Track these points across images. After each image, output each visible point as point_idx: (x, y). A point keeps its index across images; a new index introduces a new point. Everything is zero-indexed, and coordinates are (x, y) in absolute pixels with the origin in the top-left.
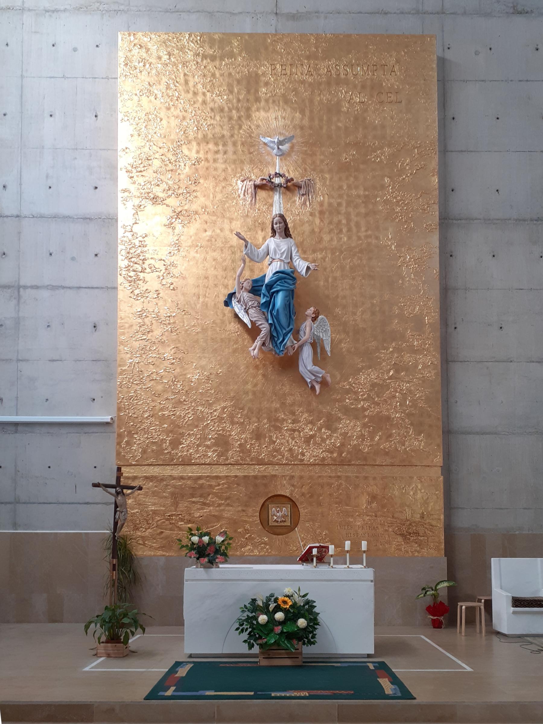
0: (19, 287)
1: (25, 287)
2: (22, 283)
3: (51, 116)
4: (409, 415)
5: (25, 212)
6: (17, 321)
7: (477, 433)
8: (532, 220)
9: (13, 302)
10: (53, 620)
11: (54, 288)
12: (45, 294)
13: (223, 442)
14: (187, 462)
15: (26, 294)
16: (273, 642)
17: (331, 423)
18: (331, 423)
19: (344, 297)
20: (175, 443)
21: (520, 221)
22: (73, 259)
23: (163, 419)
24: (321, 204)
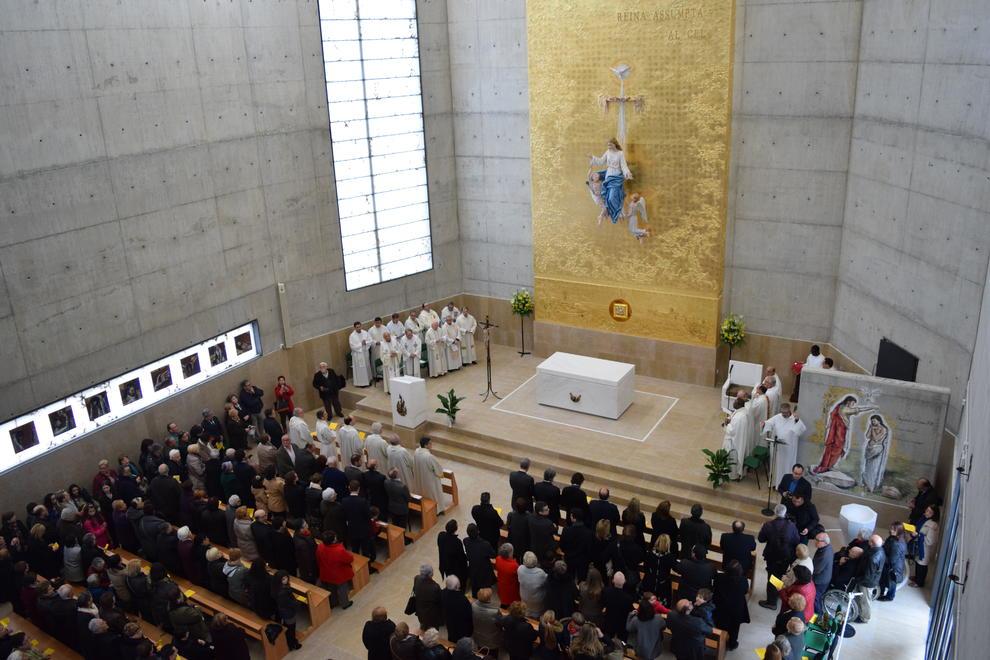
0: (484, 157)
1: (487, 157)
2: (485, 154)
3: (175, 238)
4: (701, 259)
5: (485, 111)
6: (484, 179)
7: (751, 269)
8: (804, 116)
9: (482, 166)
10: (509, 345)
11: (501, 158)
12: (497, 161)
13: (589, 265)
14: (569, 274)
15: (487, 161)
16: (510, 545)
17: (652, 260)
18: (652, 260)
19: (662, 178)
20: (564, 263)
21: (795, 117)
22: (510, 140)
23: (557, 248)
24: (249, 501)
